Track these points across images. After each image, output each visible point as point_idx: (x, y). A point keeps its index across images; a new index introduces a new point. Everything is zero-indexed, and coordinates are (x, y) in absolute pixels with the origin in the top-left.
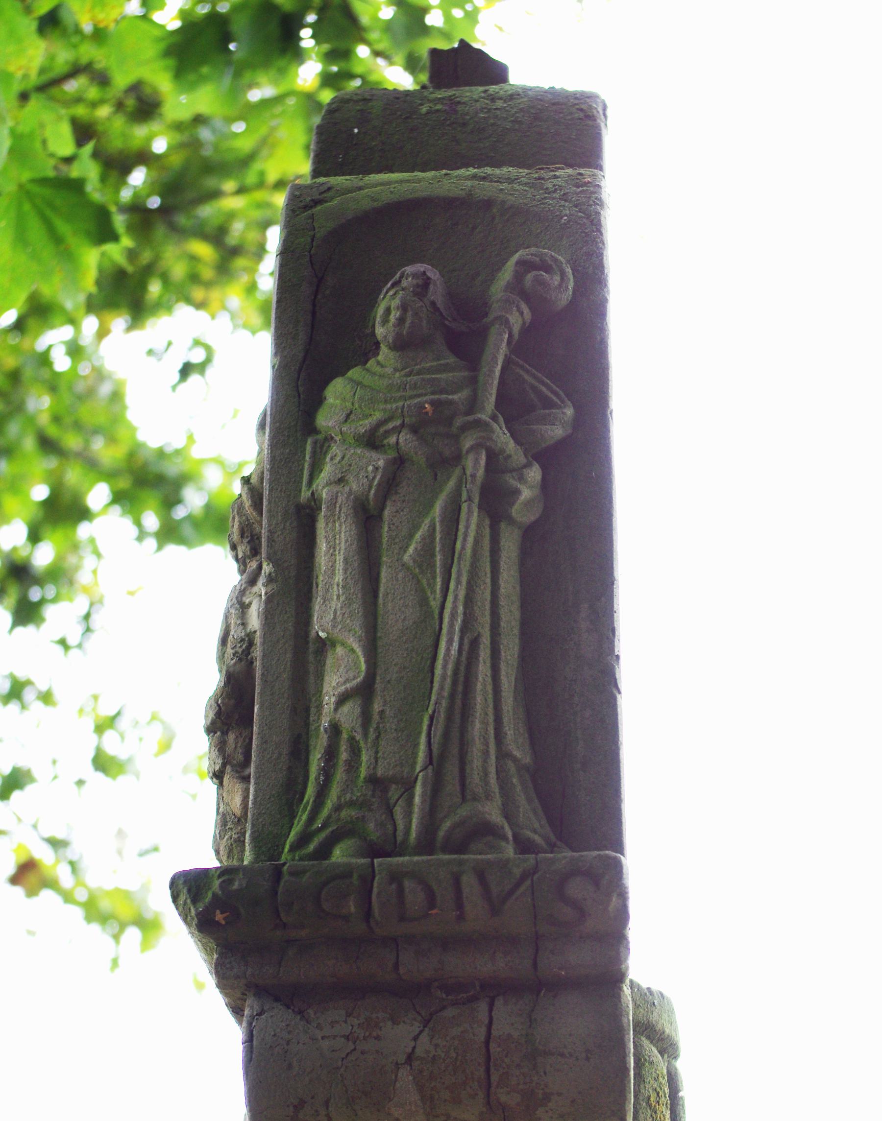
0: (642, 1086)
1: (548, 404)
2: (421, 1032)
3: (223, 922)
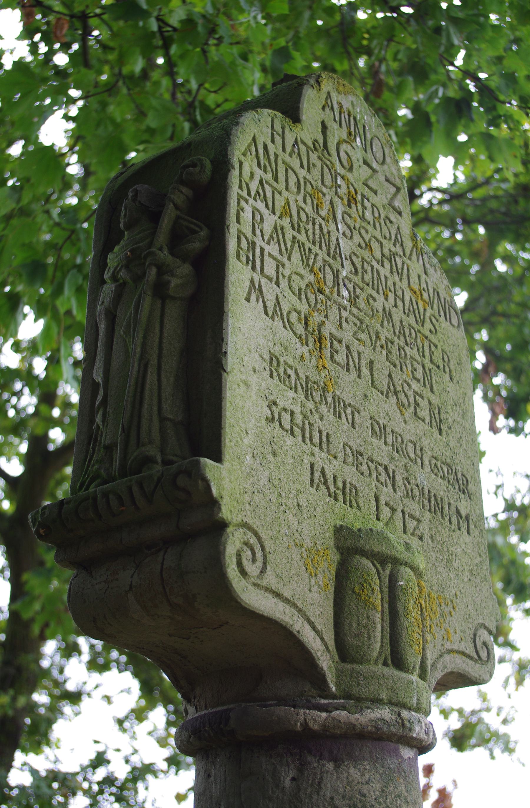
0: (348, 582)
1: (195, 232)
2: (135, 572)
3: (43, 534)
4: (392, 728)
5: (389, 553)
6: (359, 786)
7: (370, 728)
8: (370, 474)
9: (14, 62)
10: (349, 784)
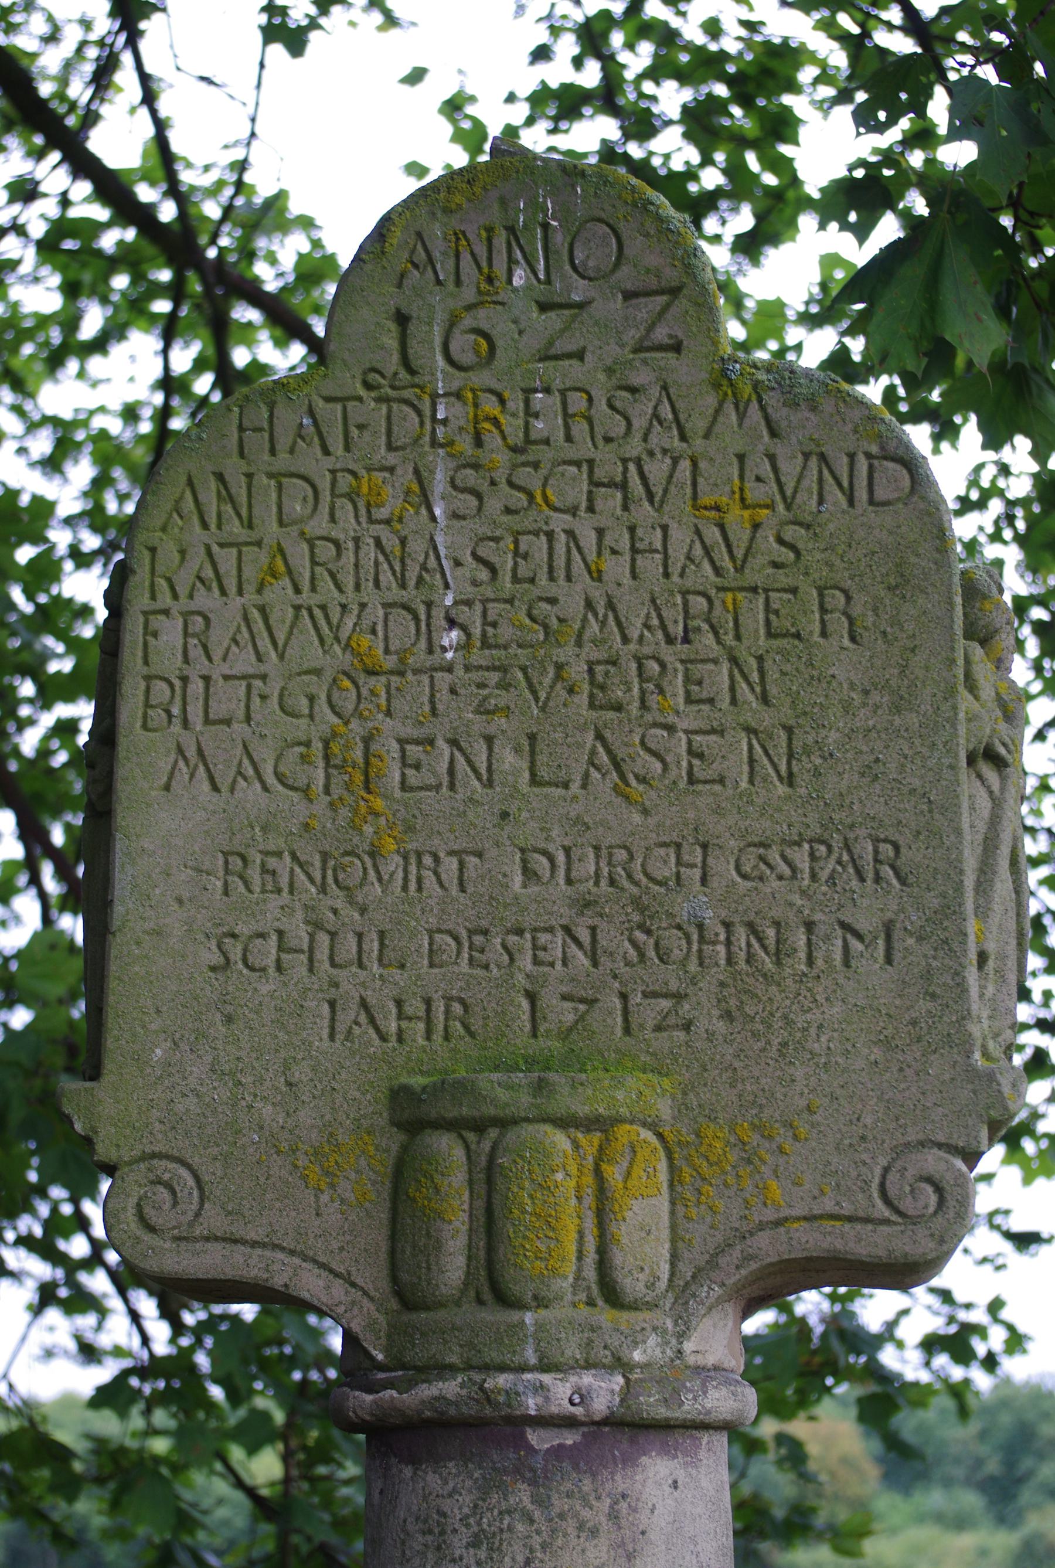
4: (464, 1410)
5: (476, 1113)
6: (439, 1501)
7: (428, 1413)
8: (642, 955)
9: (1030, 453)
10: (425, 1498)
